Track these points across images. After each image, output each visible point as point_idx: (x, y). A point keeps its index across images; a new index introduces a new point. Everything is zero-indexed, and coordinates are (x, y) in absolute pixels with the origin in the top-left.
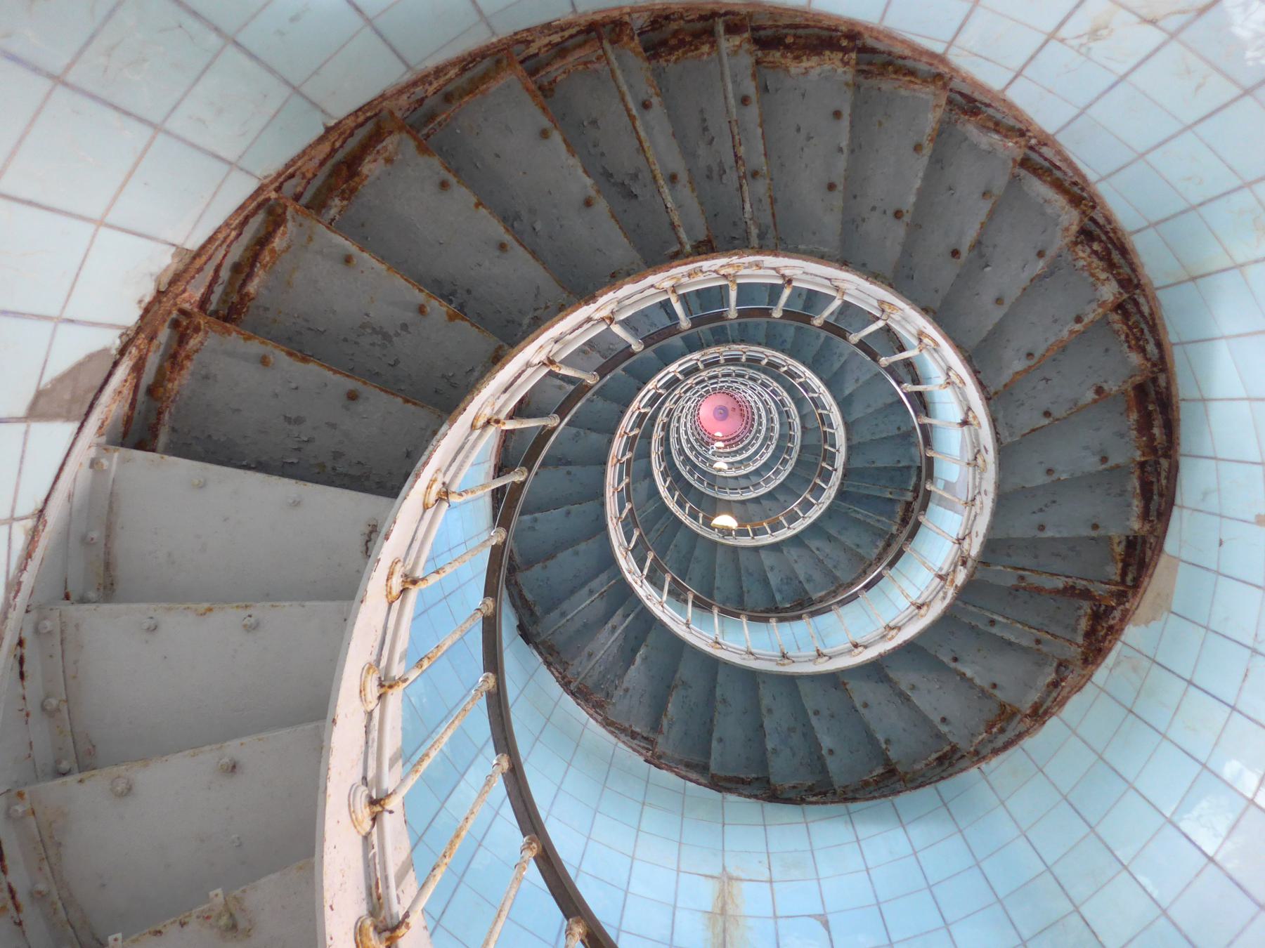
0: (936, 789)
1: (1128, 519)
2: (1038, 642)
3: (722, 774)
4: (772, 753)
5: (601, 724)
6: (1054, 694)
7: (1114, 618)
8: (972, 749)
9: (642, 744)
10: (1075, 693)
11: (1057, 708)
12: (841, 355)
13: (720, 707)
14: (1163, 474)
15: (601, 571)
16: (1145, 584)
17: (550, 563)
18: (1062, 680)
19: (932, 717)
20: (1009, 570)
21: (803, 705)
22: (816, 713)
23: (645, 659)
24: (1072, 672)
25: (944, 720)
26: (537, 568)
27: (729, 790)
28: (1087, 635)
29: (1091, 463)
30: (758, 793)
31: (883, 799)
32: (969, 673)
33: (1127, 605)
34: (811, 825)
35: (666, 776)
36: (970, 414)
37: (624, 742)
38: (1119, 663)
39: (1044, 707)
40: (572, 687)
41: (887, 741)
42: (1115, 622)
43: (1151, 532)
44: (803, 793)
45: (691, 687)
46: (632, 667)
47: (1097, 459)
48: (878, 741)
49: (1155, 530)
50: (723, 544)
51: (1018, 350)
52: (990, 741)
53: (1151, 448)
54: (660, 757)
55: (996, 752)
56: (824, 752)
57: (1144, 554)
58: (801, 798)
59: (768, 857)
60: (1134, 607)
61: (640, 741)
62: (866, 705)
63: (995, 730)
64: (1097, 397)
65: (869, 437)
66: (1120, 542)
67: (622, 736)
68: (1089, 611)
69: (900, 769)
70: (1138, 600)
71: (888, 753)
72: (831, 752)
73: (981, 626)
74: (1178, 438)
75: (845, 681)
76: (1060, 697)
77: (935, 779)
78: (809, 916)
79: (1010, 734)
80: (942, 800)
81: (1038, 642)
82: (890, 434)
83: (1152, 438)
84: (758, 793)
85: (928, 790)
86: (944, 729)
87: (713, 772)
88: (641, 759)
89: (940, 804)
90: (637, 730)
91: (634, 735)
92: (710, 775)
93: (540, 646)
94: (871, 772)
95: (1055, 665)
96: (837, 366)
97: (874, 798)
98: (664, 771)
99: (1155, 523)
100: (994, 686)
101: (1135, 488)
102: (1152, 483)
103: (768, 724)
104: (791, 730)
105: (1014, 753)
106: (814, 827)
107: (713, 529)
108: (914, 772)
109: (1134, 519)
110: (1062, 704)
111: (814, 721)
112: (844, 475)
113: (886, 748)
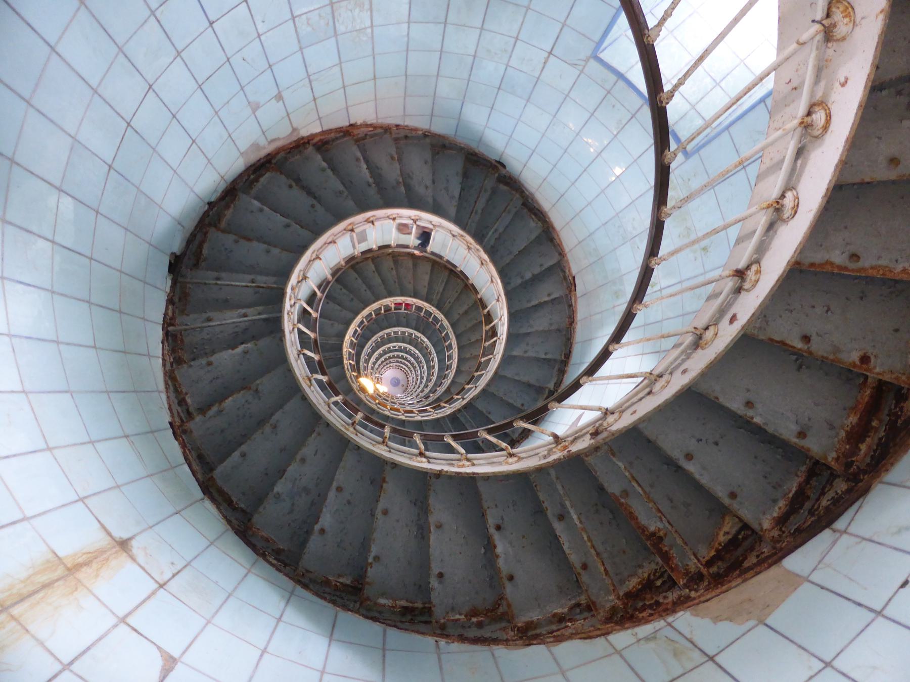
0: (385, 631)
1: (764, 514)
2: (585, 567)
3: (220, 482)
4: (275, 496)
5: (165, 374)
6: (554, 627)
7: (665, 597)
8: (442, 621)
9: (182, 415)
10: (581, 639)
11: (552, 640)
12: (531, 326)
13: (267, 428)
14: (831, 494)
15: (274, 275)
16: (734, 584)
17: (242, 241)
18: (570, 620)
19: (433, 565)
20: (627, 474)
21: (334, 474)
22: (339, 489)
23: (246, 352)
24: (585, 619)
25: (441, 575)
26: (231, 238)
27: (213, 500)
28: (629, 595)
29: (787, 431)
30: (234, 521)
31: (330, 605)
32: (499, 550)
33: (693, 594)
34: (250, 574)
35: (174, 448)
36: (754, 268)
37: (168, 397)
38: (655, 638)
39: (538, 631)
40: (171, 328)
41: (377, 558)
42: (666, 601)
43: (774, 541)
44: (270, 551)
45: (260, 399)
46: (230, 351)
47: (794, 428)
48: (369, 551)
49: (779, 541)
50: (355, 393)
51: (847, 244)
52: (463, 627)
53: (847, 460)
54: (185, 432)
55: (463, 639)
56: (317, 527)
57: (745, 558)
58: (264, 552)
59: (185, 566)
60: (702, 599)
61: (182, 411)
62: (385, 512)
63: (474, 620)
64: (858, 363)
65: (501, 395)
66: (728, 533)
67: (172, 395)
68: (646, 575)
69: (368, 591)
70: (714, 594)
71: (369, 569)
72: (322, 531)
73: (549, 513)
74: (892, 464)
75: (387, 479)
76: (559, 633)
77: (389, 622)
78: (159, 648)
79: (486, 633)
80: (384, 644)
81: (585, 567)
82: (515, 404)
83: (855, 450)
84: (234, 521)
85: (377, 627)
86: (434, 583)
87: (214, 476)
88: (168, 418)
89: (380, 646)
90: (189, 400)
91: (182, 402)
92: (210, 476)
93: (178, 285)
94: (339, 576)
95: (573, 602)
96: (523, 330)
97: (325, 599)
98: (176, 443)
99: (784, 535)
100: (511, 578)
101: (790, 491)
102: (808, 498)
103: (292, 470)
104: (306, 490)
105: (481, 653)
106: (252, 579)
107: (357, 382)
108: (376, 604)
109: (768, 517)
110: (559, 639)
111: (332, 494)
112: (465, 407)
113: (371, 564)
